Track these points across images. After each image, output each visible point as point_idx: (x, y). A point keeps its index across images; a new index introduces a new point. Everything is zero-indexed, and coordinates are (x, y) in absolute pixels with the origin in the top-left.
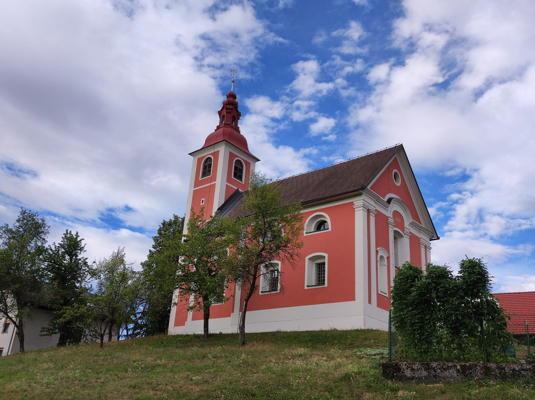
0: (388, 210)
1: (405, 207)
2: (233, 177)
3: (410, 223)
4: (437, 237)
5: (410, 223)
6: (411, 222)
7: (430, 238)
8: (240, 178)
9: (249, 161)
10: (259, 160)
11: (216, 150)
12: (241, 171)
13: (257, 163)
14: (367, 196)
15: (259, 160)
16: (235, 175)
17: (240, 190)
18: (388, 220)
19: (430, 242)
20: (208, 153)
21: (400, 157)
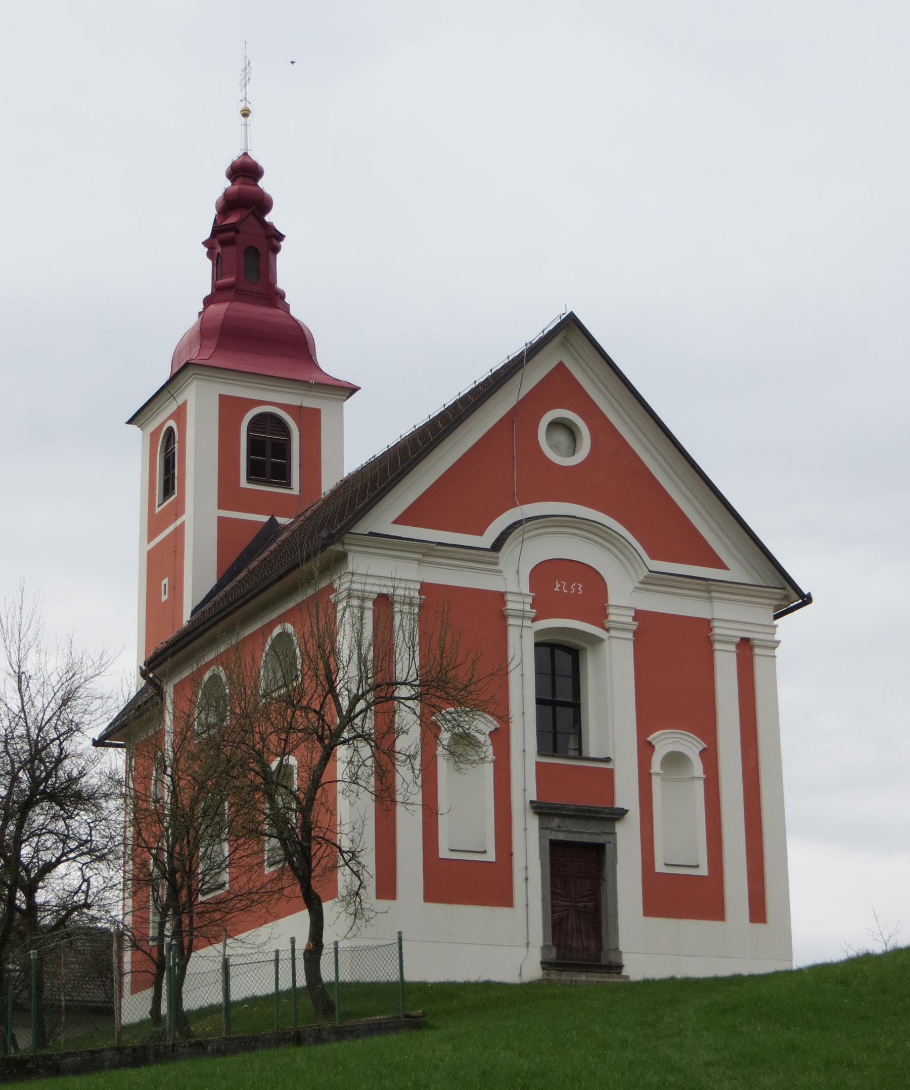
0: (501, 572)
1: (606, 536)
2: (244, 483)
3: (641, 583)
4: (797, 597)
5: (641, 583)
6: (641, 578)
7: (777, 608)
8: (282, 475)
9: (309, 402)
10: (351, 390)
11: (180, 401)
12: (283, 450)
13: (350, 404)
14: (362, 552)
15: (351, 390)
16: (256, 472)
17: (282, 521)
18: (504, 603)
19: (776, 622)
20: (163, 418)
21: (580, 356)
